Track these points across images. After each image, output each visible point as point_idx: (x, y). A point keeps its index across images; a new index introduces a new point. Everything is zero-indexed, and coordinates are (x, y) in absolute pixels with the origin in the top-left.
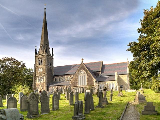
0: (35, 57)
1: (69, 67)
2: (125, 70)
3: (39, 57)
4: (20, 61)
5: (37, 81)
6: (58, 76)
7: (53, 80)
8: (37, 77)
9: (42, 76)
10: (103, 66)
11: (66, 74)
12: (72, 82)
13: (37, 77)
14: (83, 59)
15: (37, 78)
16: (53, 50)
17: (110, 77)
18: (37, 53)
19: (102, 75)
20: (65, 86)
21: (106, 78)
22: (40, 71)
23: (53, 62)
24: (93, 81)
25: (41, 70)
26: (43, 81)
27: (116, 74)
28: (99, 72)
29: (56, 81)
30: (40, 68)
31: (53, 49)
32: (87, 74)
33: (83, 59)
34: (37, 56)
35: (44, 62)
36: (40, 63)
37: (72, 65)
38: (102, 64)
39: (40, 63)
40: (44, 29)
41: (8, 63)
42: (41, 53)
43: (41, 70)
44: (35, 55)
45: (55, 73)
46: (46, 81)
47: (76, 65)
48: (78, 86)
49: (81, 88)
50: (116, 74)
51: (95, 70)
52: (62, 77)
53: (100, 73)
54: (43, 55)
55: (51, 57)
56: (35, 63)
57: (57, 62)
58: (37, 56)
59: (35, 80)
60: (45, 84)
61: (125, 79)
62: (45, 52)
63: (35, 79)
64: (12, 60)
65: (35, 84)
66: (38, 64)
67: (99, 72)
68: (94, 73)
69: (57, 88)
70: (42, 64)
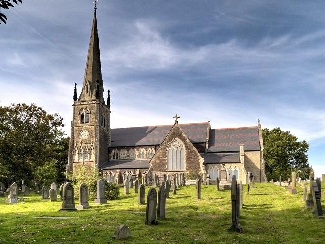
0: (74, 105)
1: (142, 132)
2: (256, 142)
3: (81, 106)
4: (49, 113)
5: (76, 158)
6: (120, 148)
7: (108, 158)
8: (76, 148)
9: (87, 148)
10: (212, 132)
11: (137, 144)
12: (155, 161)
13: (76, 148)
14: (178, 116)
15: (77, 152)
16: (109, 93)
17: (229, 155)
18: (78, 97)
19: (212, 149)
20: (138, 170)
21: (221, 157)
22: (83, 136)
23: (109, 118)
24: (199, 163)
25: (85, 135)
26: (90, 158)
27: (241, 149)
28: (206, 143)
29: (114, 158)
30: (83, 130)
31: (109, 91)
32: (187, 147)
33: (178, 116)
34: (78, 104)
35: (93, 118)
36: (85, 119)
37: (146, 128)
38: (208, 128)
39: (85, 119)
40: (93, 50)
41: (23, 117)
42: (86, 99)
43: (85, 135)
44: (72, 102)
45: (112, 143)
46: (96, 158)
47: (156, 127)
48: (166, 170)
49: (182, 176)
50: (241, 149)
51: (197, 139)
52: (128, 150)
53: (207, 145)
54: (91, 102)
55: (105, 108)
56: (74, 119)
57: (119, 120)
58: (78, 104)
59: (71, 156)
60: (93, 164)
61: (257, 159)
62: (94, 97)
63: (71, 152)
64: (31, 110)
65: (72, 163)
66: (79, 122)
67: (206, 143)
68: (196, 145)
69: (120, 173)
70: (87, 122)
